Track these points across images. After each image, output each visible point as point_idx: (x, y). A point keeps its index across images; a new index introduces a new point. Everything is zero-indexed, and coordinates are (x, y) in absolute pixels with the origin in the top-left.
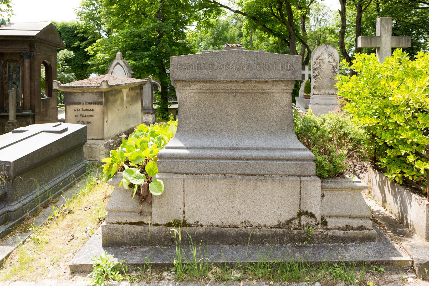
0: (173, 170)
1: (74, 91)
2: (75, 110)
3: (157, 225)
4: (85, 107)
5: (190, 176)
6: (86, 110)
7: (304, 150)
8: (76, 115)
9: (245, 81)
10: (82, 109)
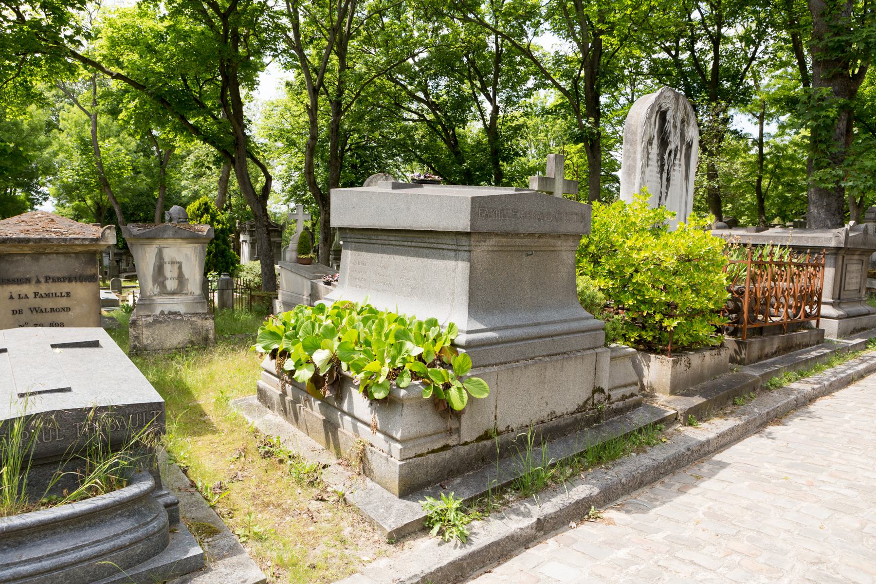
0: (481, 363)
1: (14, 250)
2: (11, 298)
3: (466, 443)
4: (43, 288)
5: (503, 367)
6: (47, 295)
7: (587, 318)
8: (17, 308)
9: (541, 236)
10: (36, 294)
